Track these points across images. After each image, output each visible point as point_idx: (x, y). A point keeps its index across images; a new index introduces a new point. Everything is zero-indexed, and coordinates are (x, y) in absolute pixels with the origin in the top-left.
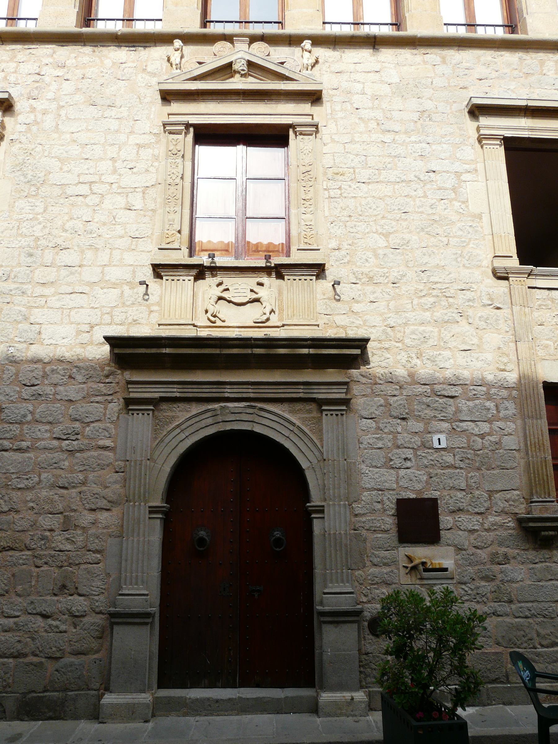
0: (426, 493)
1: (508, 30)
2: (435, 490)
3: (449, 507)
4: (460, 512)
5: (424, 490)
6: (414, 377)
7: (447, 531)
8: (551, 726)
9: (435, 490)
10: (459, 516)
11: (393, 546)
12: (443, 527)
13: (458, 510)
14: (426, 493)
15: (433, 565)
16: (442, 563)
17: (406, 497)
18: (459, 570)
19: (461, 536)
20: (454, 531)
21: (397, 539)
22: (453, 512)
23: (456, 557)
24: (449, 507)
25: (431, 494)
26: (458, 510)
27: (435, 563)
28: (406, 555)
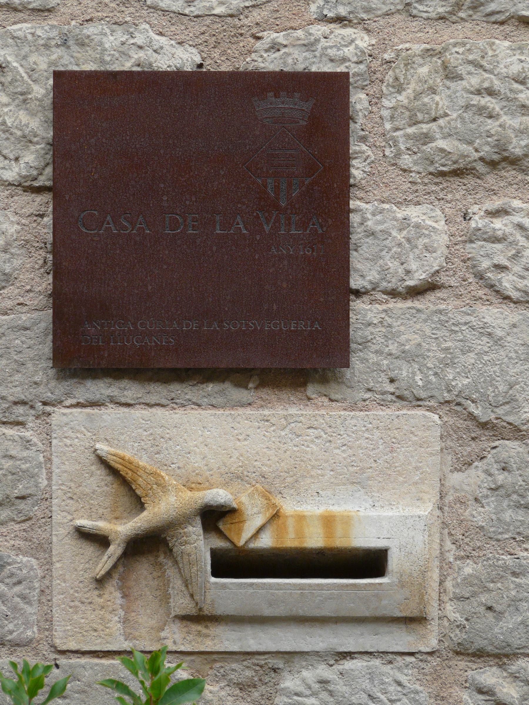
0: (270, 36)
1: (339, 531)
2: (339, 20)
3: (427, 138)
4: (510, 174)
5: (256, 15)
6: (366, 221)
7: (400, 305)
8: (348, 283)
9: (339, 20)
10: (496, 203)
11: (18, 393)
12: (373, 275)
13: (493, 164)
14: (270, 36)
15: (281, 533)
16: (347, 520)
17: (128, 66)
18: (468, 570)
19: (498, 342)
20: (449, 306)
21: (47, 348)
22: (457, 173)
23: (456, 478)
24: (427, 138)
25: (309, 46)
26: (493, 164)
27: (301, 518)
28: (103, 462)
